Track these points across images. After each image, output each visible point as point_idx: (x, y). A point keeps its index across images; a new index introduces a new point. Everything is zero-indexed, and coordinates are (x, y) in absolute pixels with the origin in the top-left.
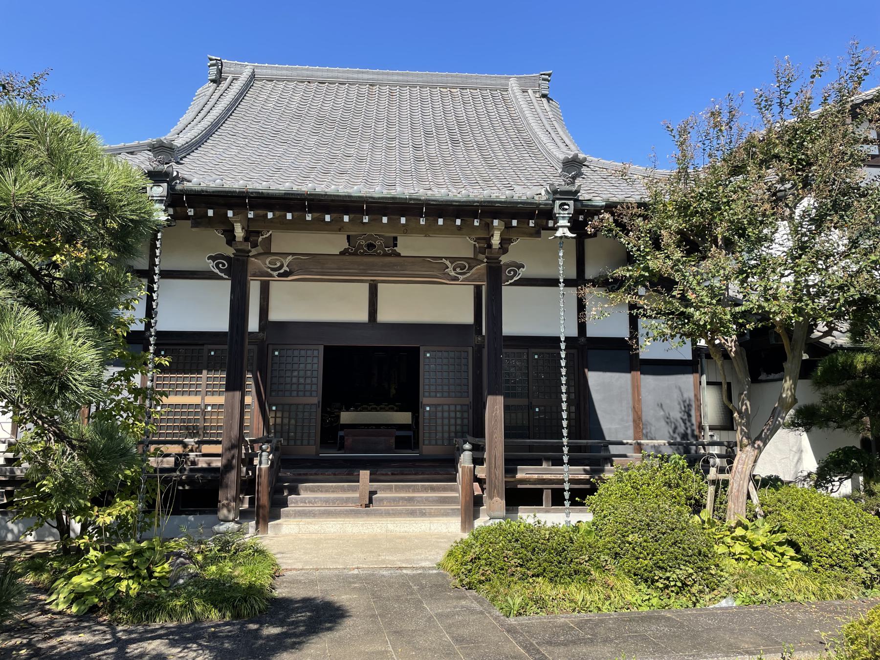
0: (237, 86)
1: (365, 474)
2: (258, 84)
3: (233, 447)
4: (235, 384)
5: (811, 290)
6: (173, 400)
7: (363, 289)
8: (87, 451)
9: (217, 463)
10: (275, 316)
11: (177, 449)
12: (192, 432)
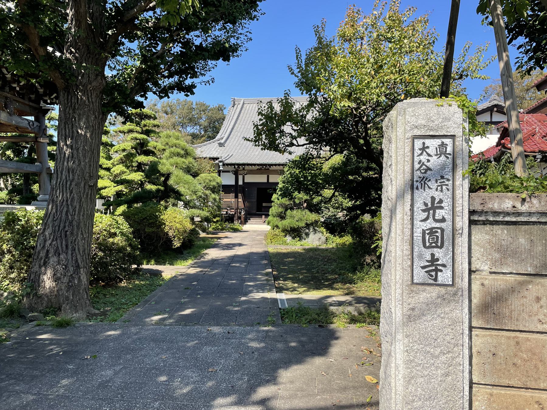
0: (240, 106)
1: (263, 216)
2: (245, 105)
3: (236, 209)
4: (236, 197)
5: (405, 237)
6: (225, 200)
7: (266, 176)
8: (217, 206)
9: (234, 213)
10: (246, 181)
11: (226, 210)
12: (229, 207)
